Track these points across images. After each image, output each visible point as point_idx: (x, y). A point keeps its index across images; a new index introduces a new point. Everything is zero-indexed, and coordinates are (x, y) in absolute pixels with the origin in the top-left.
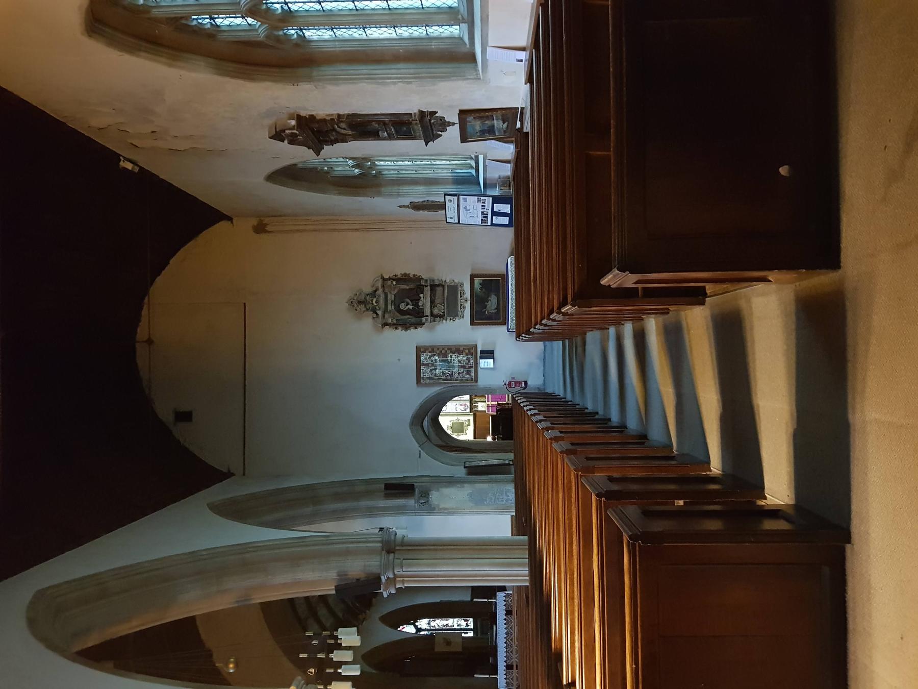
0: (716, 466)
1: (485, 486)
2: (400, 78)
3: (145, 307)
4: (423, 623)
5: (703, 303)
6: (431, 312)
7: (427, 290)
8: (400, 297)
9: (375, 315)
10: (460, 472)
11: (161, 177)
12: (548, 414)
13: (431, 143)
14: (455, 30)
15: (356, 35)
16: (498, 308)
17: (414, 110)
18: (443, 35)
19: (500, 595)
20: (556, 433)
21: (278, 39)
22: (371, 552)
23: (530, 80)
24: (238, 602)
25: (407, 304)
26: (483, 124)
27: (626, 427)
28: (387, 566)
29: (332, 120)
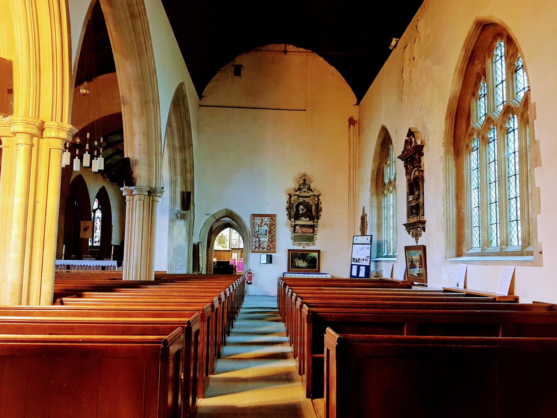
0: (202, 402)
2: (447, 209)
3: (305, 50)
4: (99, 214)
5: (308, 396)
6: (297, 225)
7: (311, 223)
8: (308, 206)
9: (296, 189)
10: (196, 240)
11: (386, 63)
12: (233, 296)
13: (405, 227)
14: (476, 244)
15: (473, 183)
16: (299, 267)
17: (426, 218)
18: (474, 237)
19: (115, 263)
20: (223, 299)
21: (471, 135)
22: (150, 181)
23: (445, 291)
24: (123, 98)
25: (303, 210)
26: (416, 261)
27: (224, 345)
28: (140, 190)
29: (420, 167)
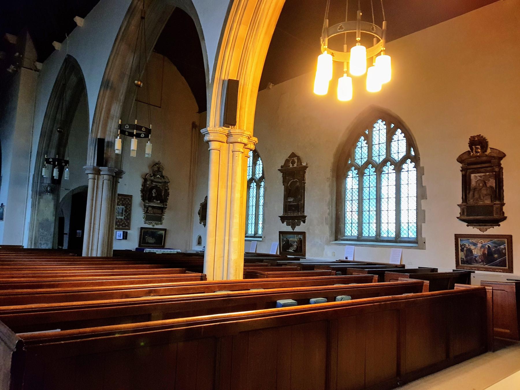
1: (52, 230)
8: (159, 191)
16: (148, 243)
